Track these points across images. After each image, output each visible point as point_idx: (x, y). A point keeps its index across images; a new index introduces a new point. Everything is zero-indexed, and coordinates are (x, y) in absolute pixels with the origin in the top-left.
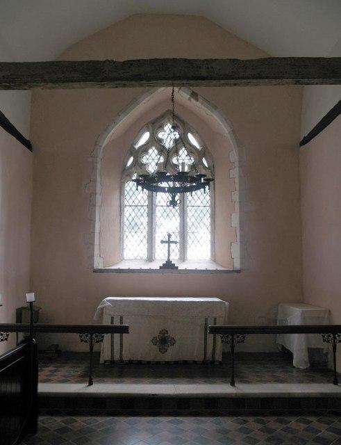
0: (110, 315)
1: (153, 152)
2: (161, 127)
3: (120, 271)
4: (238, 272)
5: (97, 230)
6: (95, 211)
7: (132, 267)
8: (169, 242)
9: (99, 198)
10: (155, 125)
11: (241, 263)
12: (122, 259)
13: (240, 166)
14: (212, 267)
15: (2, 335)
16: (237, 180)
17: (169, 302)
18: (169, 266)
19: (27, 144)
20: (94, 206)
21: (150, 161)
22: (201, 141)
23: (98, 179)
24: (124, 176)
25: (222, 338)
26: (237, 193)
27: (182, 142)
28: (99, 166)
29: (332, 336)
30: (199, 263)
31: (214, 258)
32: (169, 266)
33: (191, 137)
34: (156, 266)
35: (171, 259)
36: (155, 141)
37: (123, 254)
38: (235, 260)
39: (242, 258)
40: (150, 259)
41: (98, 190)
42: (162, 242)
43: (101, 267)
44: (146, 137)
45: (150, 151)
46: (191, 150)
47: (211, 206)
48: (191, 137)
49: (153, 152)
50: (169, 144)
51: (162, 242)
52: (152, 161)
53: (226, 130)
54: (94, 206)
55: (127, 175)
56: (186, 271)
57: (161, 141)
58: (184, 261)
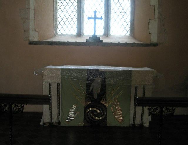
0: (47, 82)
3: (52, 43)
4: (155, 45)
5: (32, 6)
8: (95, 18)
11: (158, 37)
12: (56, 34)
14: (131, 41)
17: (91, 70)
25: (149, 110)
29: (159, 109)
40: (80, 34)
42: (89, 18)
43: (36, 39)
51: (89, 18)
58: (107, 36)
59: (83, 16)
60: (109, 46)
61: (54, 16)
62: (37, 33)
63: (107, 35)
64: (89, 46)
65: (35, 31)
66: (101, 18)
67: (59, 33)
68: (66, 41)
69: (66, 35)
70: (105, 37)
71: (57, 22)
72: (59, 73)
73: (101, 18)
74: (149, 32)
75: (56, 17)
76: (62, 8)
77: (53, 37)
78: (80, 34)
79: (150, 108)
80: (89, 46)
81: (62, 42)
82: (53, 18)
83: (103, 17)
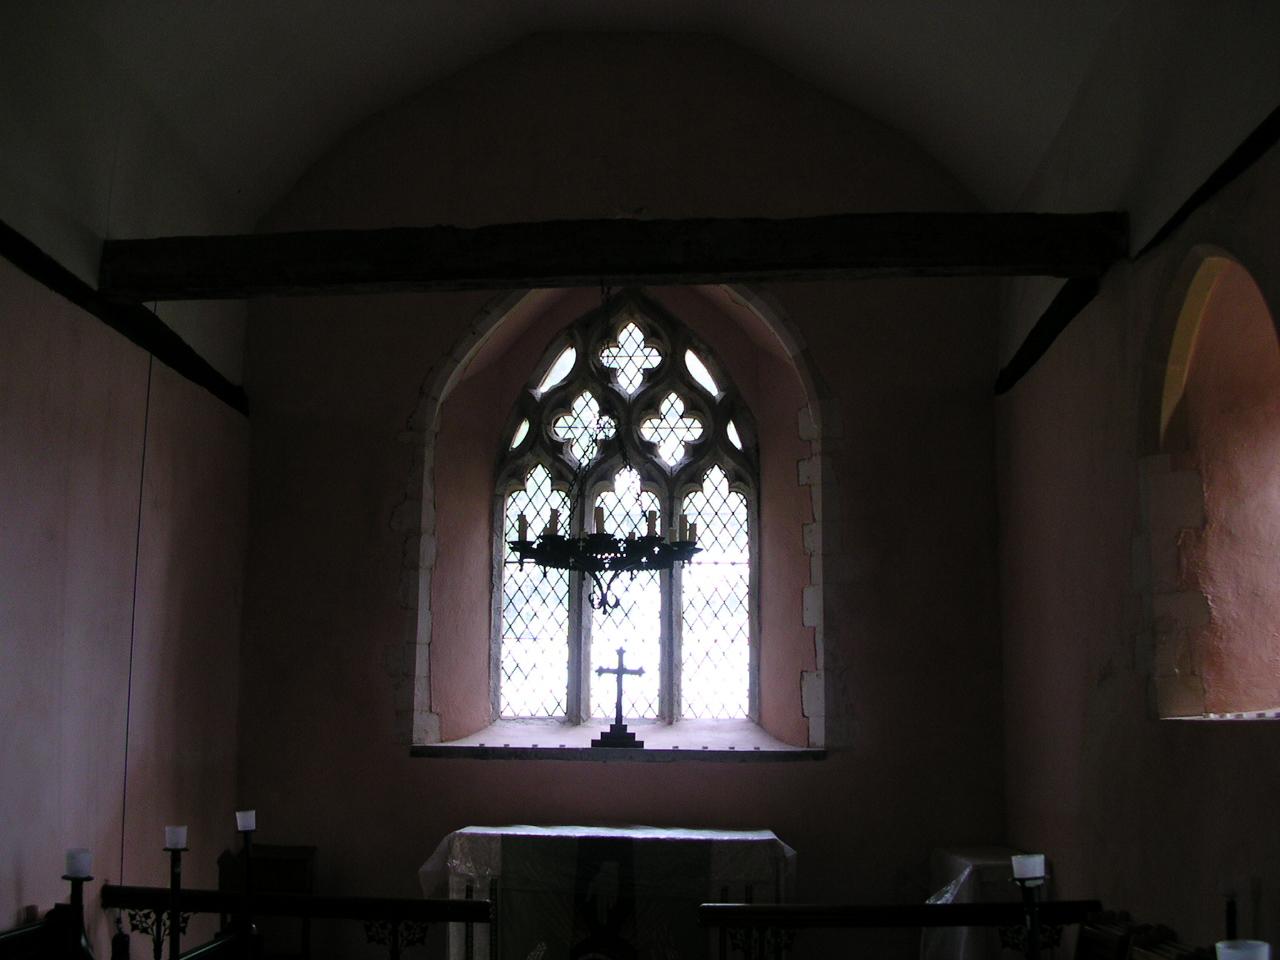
1: (587, 407)
2: (610, 338)
3: (483, 753)
4: (817, 756)
5: (421, 668)
7: (515, 743)
9: (428, 548)
10: (596, 334)
11: (829, 731)
12: (496, 715)
14: (746, 741)
15: (121, 945)
16: (817, 493)
18: (618, 737)
19: (232, 395)
20: (415, 567)
21: (577, 433)
23: (428, 490)
25: (132, 917)
26: (817, 528)
27: (666, 378)
28: (429, 455)
29: (153, 916)
30: (713, 729)
31: (758, 715)
32: (618, 737)
33: (696, 368)
34: (580, 739)
36: (593, 377)
37: (496, 703)
39: (831, 716)
40: (576, 713)
43: (432, 741)
44: (565, 363)
45: (578, 404)
46: (696, 403)
47: (751, 563)
48: (696, 368)
49: (587, 407)
50: (629, 383)
53: (788, 352)
56: (675, 755)
58: (670, 723)
59: (588, 654)
60: (669, 762)
61: (490, 655)
62: (435, 717)
63: (667, 719)
64: (605, 762)
65: (431, 711)
66: (601, 671)
67: (507, 713)
68: (528, 744)
69: (531, 719)
70: (664, 727)
71: (499, 676)
72: (497, 846)
73: (601, 671)
74: (803, 709)
75: (498, 659)
76: (519, 627)
77: (486, 727)
78: (576, 713)
79: (133, 913)
80: (605, 762)
81: (516, 750)
82: (486, 664)
83: (593, 675)
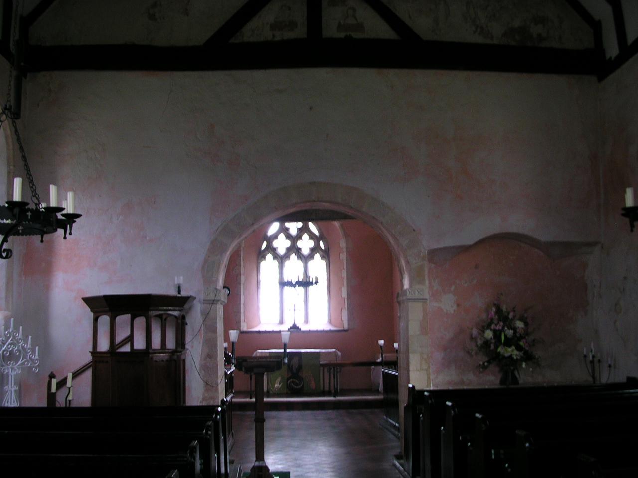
3: (259, 332)
4: (346, 331)
5: (242, 311)
6: (240, 288)
9: (243, 278)
11: (349, 324)
13: (347, 252)
18: (294, 328)
22: (319, 229)
23: (242, 263)
24: (260, 257)
27: (304, 229)
32: (294, 328)
35: (296, 323)
38: (344, 322)
40: (281, 322)
41: (242, 271)
46: (312, 236)
52: (282, 244)
54: (240, 284)
55: (262, 257)
57: (287, 229)
